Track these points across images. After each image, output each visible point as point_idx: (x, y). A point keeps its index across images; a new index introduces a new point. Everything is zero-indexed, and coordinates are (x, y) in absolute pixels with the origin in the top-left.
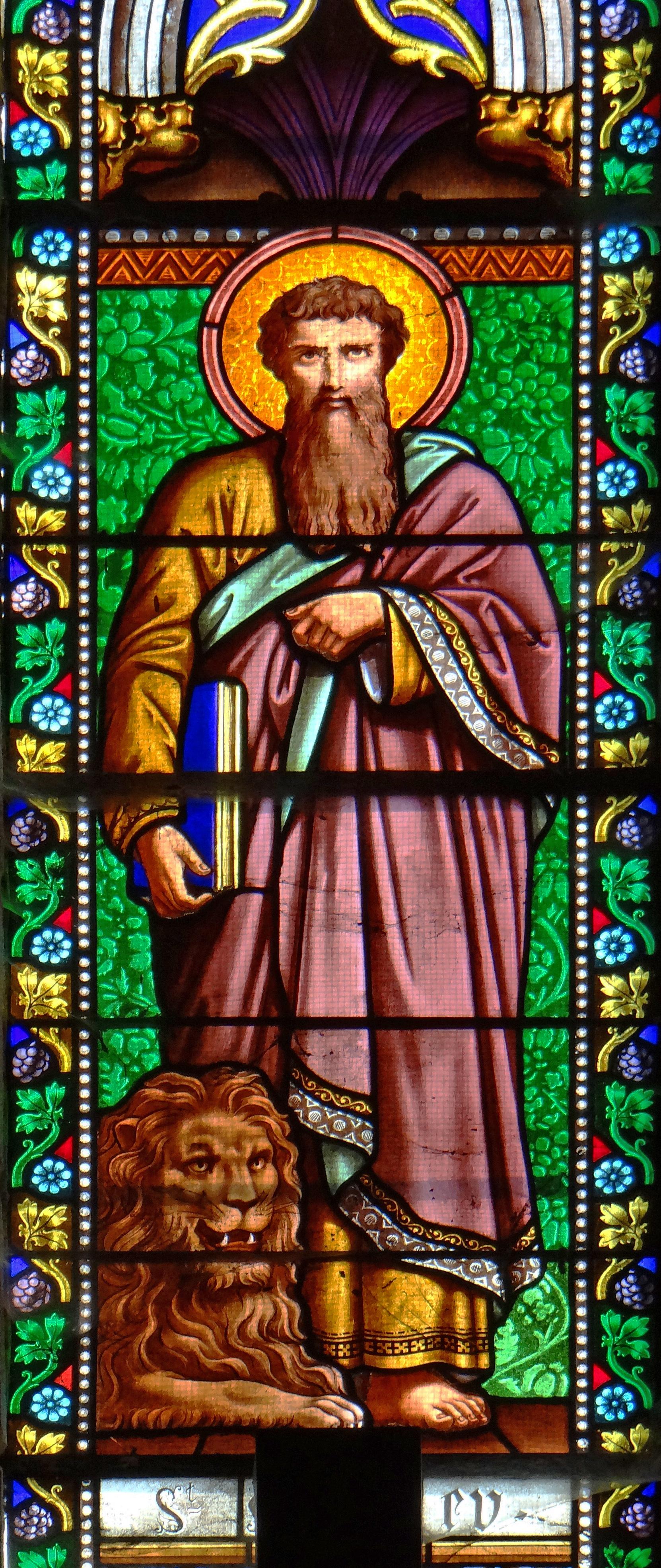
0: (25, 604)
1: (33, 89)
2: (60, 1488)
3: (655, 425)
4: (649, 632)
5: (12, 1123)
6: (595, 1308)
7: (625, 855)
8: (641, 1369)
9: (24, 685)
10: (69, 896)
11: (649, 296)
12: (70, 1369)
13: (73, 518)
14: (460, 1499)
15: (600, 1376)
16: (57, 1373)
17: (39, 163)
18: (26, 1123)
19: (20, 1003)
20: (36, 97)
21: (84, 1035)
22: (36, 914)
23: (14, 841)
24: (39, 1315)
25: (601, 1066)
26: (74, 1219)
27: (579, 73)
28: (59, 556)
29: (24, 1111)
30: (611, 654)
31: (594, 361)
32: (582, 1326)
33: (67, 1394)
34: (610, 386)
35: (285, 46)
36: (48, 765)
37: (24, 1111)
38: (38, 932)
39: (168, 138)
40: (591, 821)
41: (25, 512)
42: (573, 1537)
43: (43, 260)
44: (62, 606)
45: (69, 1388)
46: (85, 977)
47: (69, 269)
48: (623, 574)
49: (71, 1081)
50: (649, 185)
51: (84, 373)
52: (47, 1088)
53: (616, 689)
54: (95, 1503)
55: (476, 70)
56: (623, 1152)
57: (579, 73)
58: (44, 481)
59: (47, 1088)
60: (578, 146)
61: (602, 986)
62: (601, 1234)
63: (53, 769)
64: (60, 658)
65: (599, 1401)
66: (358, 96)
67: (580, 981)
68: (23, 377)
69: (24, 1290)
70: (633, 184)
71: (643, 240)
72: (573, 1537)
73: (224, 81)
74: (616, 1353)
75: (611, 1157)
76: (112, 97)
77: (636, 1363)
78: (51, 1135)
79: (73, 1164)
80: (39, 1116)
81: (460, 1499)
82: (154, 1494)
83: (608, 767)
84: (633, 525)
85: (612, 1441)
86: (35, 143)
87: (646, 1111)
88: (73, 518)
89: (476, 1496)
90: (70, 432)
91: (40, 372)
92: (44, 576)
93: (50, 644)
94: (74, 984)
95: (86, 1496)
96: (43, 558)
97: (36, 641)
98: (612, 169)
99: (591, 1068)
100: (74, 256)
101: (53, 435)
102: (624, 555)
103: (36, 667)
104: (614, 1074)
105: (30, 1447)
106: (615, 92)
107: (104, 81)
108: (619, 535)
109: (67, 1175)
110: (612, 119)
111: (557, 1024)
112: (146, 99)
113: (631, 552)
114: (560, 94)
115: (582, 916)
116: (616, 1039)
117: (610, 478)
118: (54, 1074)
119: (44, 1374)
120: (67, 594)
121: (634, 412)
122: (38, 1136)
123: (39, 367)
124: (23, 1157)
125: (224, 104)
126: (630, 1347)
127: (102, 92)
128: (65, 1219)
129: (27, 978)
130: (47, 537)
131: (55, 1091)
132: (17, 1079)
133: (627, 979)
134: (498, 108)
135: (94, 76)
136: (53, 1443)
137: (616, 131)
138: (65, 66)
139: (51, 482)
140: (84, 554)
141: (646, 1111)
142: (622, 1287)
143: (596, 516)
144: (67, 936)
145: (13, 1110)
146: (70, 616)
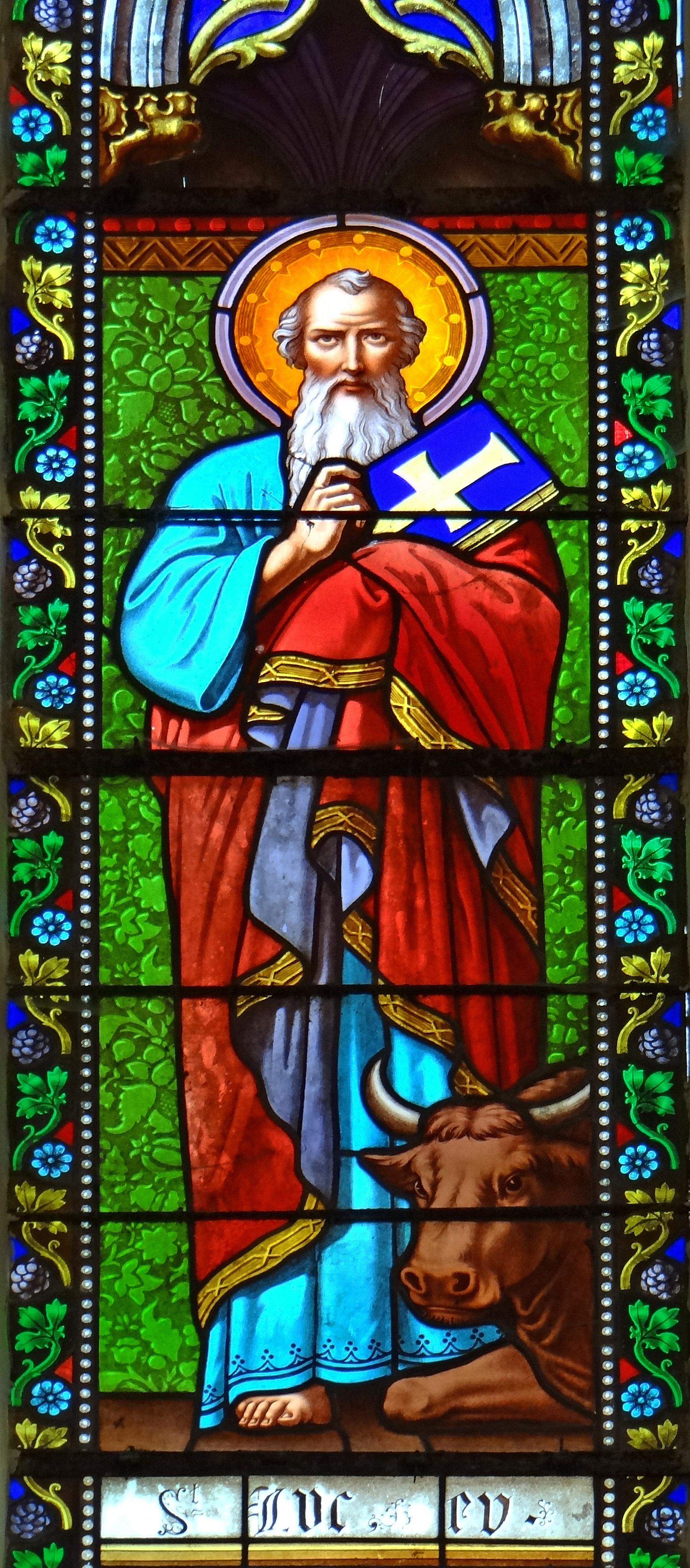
0: (23, 1285)
1: (37, 299)
2: (58, 1487)
3: (672, 408)
4: (669, 848)
5: (12, 1108)
6: (614, 830)
7: (647, 832)
8: (666, 1126)
9: (26, 1367)
10: (73, 413)
11: (667, 976)
12: (74, 429)
13: (73, 1199)
14: (467, 1501)
15: (627, 1370)
16: (60, 1125)
17: (39, 148)
18: (27, 639)
19: (24, 68)
20: (40, 84)
21: (90, 224)
22: (40, 430)
23: (15, 1287)
24: (43, 374)
25: (625, 1284)
26: (78, 275)
27: (587, 67)
28: (60, 1236)
29: (24, 1095)
30: (631, 865)
31: (611, 577)
32: (596, 161)
33: (67, 1386)
34: (628, 599)
35: (290, 42)
36: (51, 743)
37: (24, 1095)
38: (42, 450)
39: (172, 126)
40: (608, 802)
41: (30, 497)
42: (596, 1541)
43: (43, 1172)
44: (66, 357)
45: (74, 448)
46: (88, 722)
47: (74, 257)
48: (651, 1501)
49: (74, 597)
50: (660, 174)
51: (89, 357)
52: (49, 1073)
53: (636, 903)
54: (97, 1504)
55: (482, 58)
56: (650, 1374)
57: (587, 67)
58: (44, 1161)
59: (49, 1073)
60: (588, 139)
61: (625, 729)
62: (615, 71)
63: (57, 746)
64: (63, 411)
65: (624, 1397)
66: (364, 955)
67: (594, 67)
68: (23, 825)
69: (28, 347)
70: (644, 174)
71: (658, 230)
72: (596, 1541)
73: (227, 72)
74: (637, 874)
75: (637, 1380)
76: (114, 86)
77: (661, 1119)
78: (53, 652)
79: (77, 682)
80: (39, 1333)
81: (467, 1501)
82: (157, 1498)
83: (628, 746)
84: (655, 736)
85: (639, 1436)
86: (36, 129)
87: (670, 1330)
88: (73, 1199)
89: (484, 1500)
90: (73, 413)
91: (44, 583)
92: (49, 329)
93: (52, 1093)
94: (75, 964)
95: (88, 1496)
96: (43, 1237)
97: (36, 1323)
98: (624, 157)
99: (607, 816)
100: (79, 243)
101: (53, 1349)
102: (643, 535)
103: (35, 1349)
104: (634, 589)
105: (30, 1203)
106: (633, 531)
107: (105, 73)
108: (636, 512)
109: (68, 1158)
110: (630, 1026)
111: (575, 990)
112: (147, 89)
113: (650, 532)
114: (564, 88)
115: (601, 900)
116: (640, 1251)
117: (634, 1398)
118: (58, 590)
119: (50, 430)
120: (71, 569)
121: (653, 624)
122: (41, 424)
123: (43, 579)
124: (26, 444)
125: (225, 94)
126: (659, 1339)
127: (104, 82)
128: (67, 971)
129: (28, 722)
130: (47, 1216)
131: (59, 380)
132: (19, 595)
133: (641, 44)
134: (507, 98)
135: (95, 66)
136: (57, 731)
137: (636, 1277)
138: (70, 279)
139: (54, 236)
140: (85, 1439)
141: (670, 1330)
142: (648, 1276)
143: (614, 966)
144: (72, 454)
145: (15, 1095)
146: (75, 368)
